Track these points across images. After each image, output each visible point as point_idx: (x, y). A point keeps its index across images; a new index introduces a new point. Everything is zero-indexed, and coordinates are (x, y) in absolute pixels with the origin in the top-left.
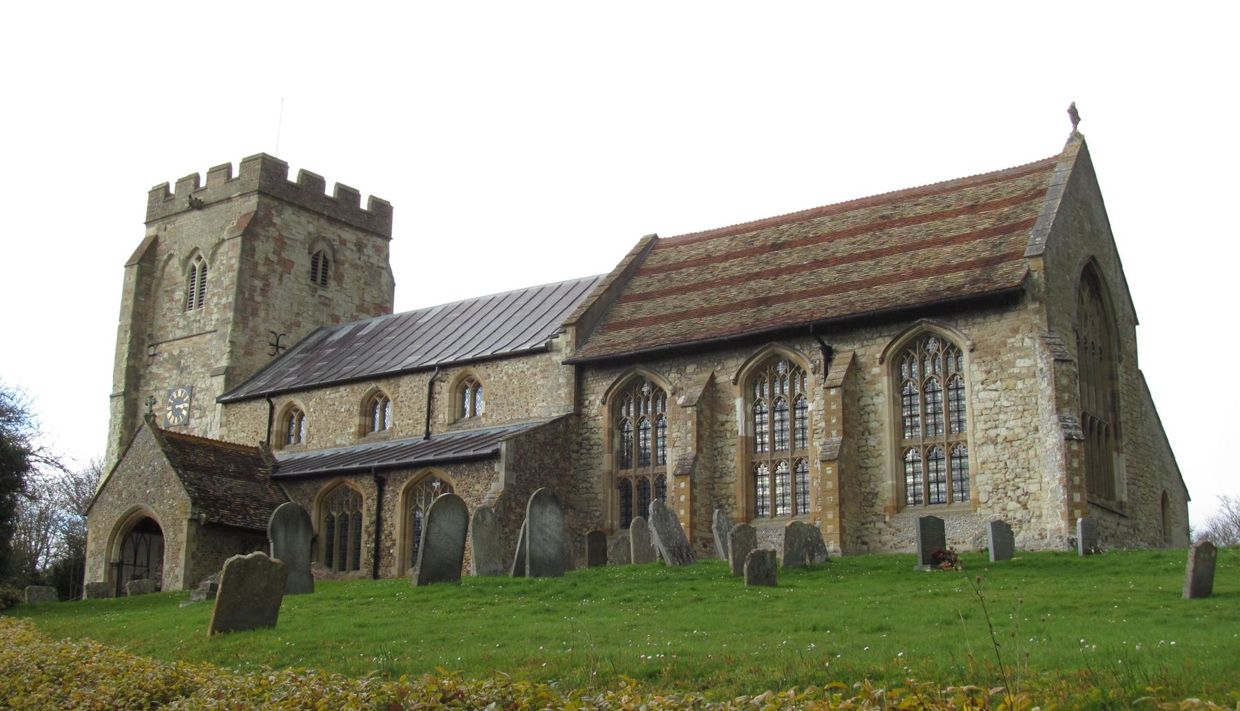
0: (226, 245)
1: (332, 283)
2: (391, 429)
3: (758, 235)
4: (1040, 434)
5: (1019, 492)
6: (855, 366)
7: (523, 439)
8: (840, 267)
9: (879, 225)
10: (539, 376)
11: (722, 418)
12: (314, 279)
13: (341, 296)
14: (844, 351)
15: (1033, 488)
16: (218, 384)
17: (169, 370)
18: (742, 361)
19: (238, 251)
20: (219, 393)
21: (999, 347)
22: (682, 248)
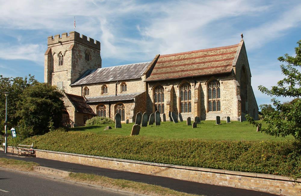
1: (90, 60)
3: (180, 56)
5: (229, 109)
9: (204, 56)
12: (86, 59)
15: (232, 109)
16: (70, 82)
22: (165, 58)
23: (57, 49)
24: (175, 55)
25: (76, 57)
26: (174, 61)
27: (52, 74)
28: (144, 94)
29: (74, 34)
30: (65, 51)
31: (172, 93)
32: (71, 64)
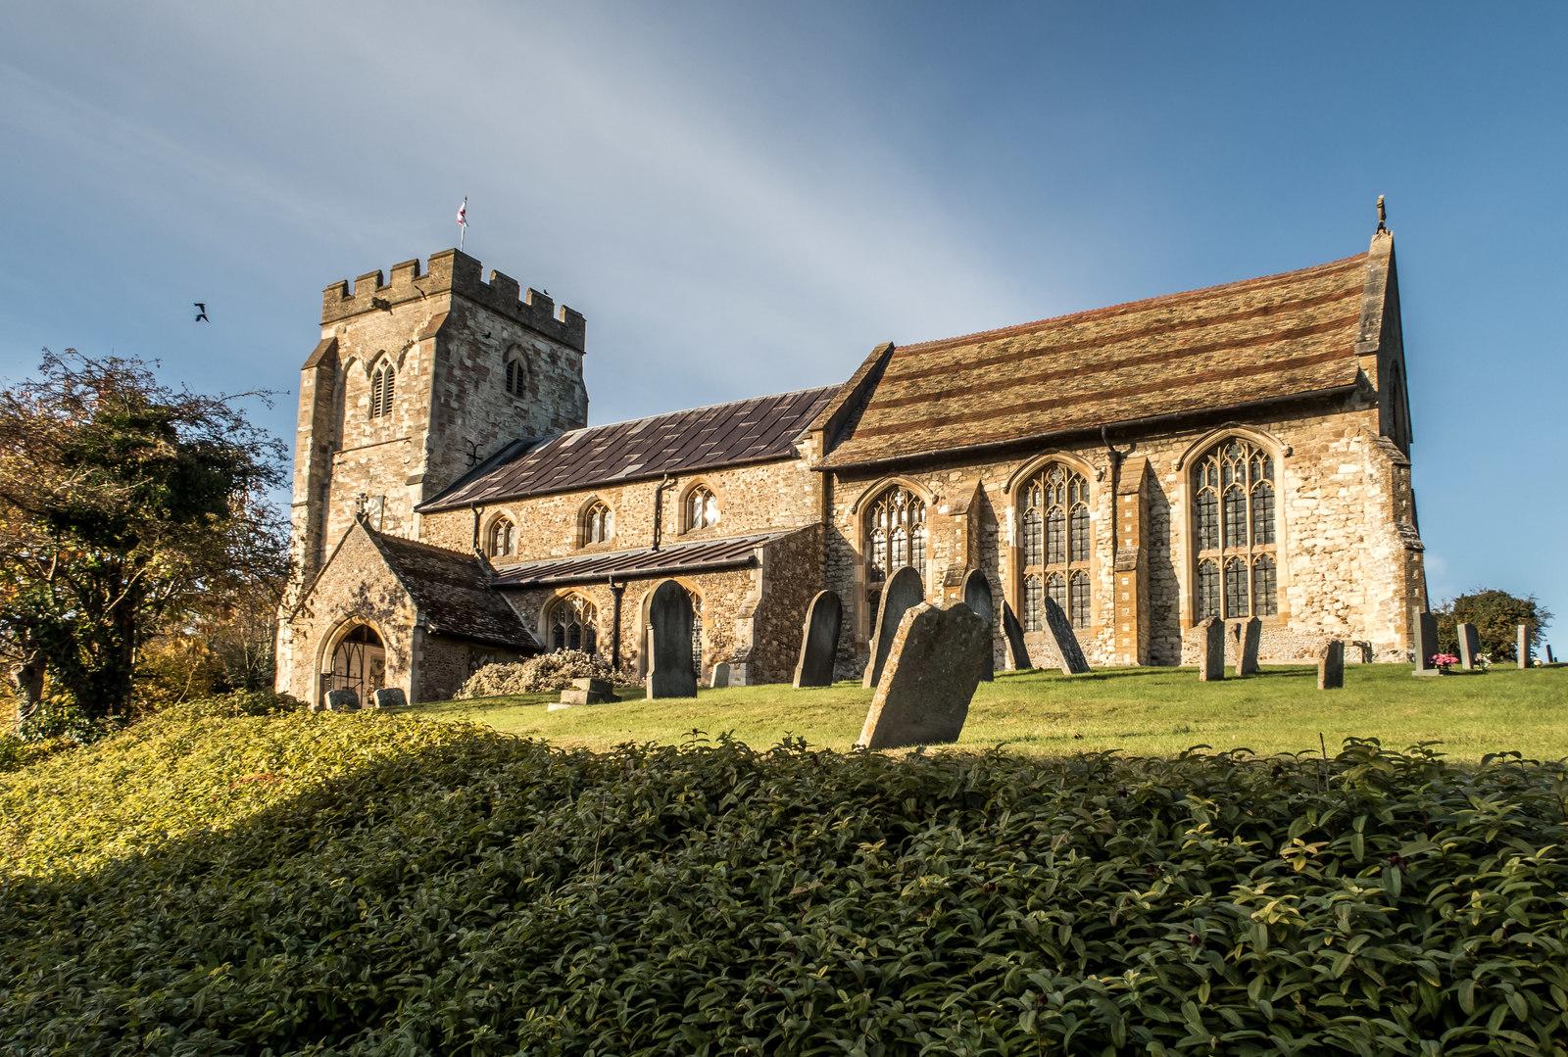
0: (416, 349)
1: (528, 394)
2: (614, 540)
3: (1011, 342)
4: (1365, 544)
5: (1338, 606)
6: (1149, 474)
7: (778, 546)
8: (1120, 370)
9: (1156, 329)
10: (782, 483)
11: (990, 528)
12: (509, 389)
13: (541, 408)
14: (1137, 457)
15: (1355, 600)
16: (416, 492)
17: (357, 480)
18: (1014, 468)
19: (432, 355)
20: (418, 502)
21: (1320, 451)
22: (924, 356)
23: (367, 336)
24: (982, 339)
25: (457, 372)
26: (980, 363)
27: (335, 461)
28: (810, 538)
29: (450, 261)
30: (398, 341)
31: (976, 522)
32: (426, 403)
